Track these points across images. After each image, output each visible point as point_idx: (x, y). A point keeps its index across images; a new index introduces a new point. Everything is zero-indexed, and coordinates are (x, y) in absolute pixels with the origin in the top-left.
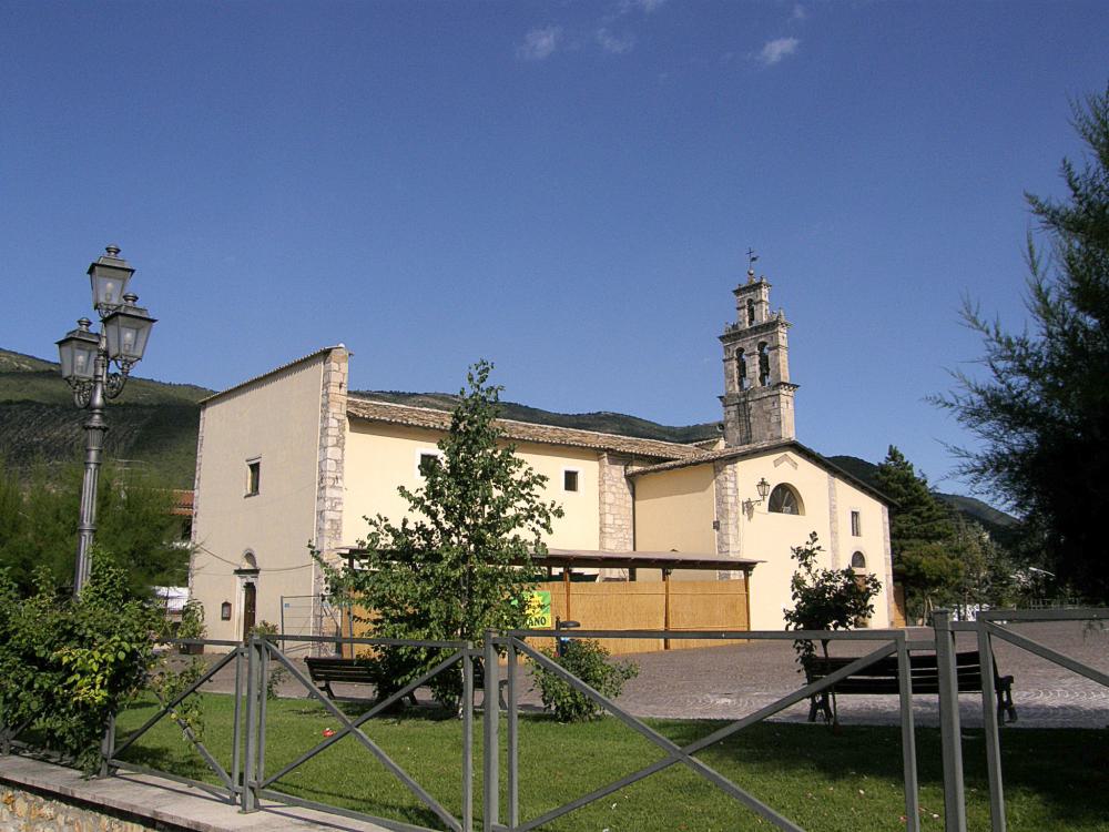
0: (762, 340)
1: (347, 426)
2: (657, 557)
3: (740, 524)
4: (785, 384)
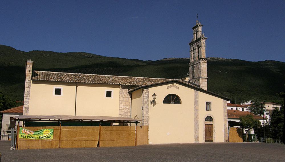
0: (198, 44)
1: (31, 82)
2: (88, 119)
3: (149, 107)
4: (202, 59)
